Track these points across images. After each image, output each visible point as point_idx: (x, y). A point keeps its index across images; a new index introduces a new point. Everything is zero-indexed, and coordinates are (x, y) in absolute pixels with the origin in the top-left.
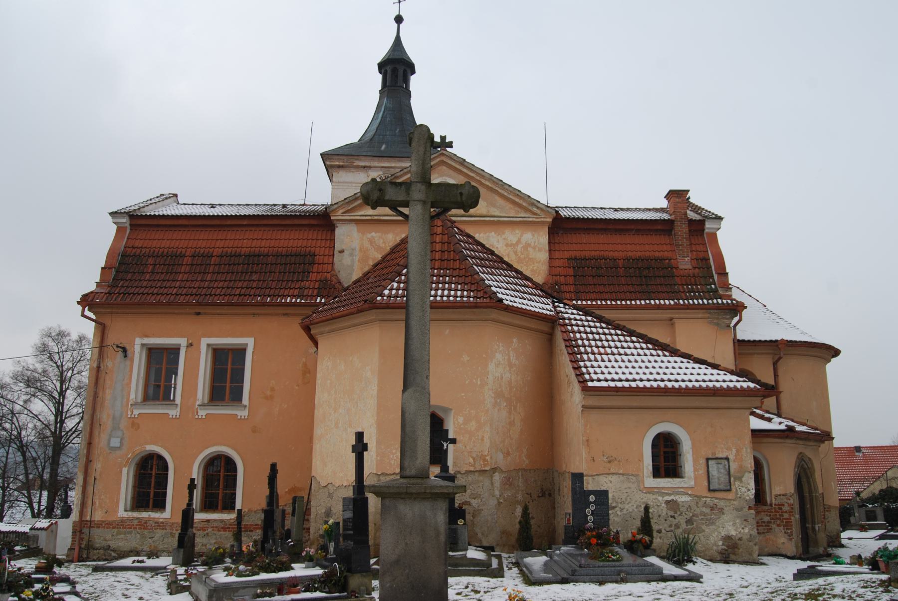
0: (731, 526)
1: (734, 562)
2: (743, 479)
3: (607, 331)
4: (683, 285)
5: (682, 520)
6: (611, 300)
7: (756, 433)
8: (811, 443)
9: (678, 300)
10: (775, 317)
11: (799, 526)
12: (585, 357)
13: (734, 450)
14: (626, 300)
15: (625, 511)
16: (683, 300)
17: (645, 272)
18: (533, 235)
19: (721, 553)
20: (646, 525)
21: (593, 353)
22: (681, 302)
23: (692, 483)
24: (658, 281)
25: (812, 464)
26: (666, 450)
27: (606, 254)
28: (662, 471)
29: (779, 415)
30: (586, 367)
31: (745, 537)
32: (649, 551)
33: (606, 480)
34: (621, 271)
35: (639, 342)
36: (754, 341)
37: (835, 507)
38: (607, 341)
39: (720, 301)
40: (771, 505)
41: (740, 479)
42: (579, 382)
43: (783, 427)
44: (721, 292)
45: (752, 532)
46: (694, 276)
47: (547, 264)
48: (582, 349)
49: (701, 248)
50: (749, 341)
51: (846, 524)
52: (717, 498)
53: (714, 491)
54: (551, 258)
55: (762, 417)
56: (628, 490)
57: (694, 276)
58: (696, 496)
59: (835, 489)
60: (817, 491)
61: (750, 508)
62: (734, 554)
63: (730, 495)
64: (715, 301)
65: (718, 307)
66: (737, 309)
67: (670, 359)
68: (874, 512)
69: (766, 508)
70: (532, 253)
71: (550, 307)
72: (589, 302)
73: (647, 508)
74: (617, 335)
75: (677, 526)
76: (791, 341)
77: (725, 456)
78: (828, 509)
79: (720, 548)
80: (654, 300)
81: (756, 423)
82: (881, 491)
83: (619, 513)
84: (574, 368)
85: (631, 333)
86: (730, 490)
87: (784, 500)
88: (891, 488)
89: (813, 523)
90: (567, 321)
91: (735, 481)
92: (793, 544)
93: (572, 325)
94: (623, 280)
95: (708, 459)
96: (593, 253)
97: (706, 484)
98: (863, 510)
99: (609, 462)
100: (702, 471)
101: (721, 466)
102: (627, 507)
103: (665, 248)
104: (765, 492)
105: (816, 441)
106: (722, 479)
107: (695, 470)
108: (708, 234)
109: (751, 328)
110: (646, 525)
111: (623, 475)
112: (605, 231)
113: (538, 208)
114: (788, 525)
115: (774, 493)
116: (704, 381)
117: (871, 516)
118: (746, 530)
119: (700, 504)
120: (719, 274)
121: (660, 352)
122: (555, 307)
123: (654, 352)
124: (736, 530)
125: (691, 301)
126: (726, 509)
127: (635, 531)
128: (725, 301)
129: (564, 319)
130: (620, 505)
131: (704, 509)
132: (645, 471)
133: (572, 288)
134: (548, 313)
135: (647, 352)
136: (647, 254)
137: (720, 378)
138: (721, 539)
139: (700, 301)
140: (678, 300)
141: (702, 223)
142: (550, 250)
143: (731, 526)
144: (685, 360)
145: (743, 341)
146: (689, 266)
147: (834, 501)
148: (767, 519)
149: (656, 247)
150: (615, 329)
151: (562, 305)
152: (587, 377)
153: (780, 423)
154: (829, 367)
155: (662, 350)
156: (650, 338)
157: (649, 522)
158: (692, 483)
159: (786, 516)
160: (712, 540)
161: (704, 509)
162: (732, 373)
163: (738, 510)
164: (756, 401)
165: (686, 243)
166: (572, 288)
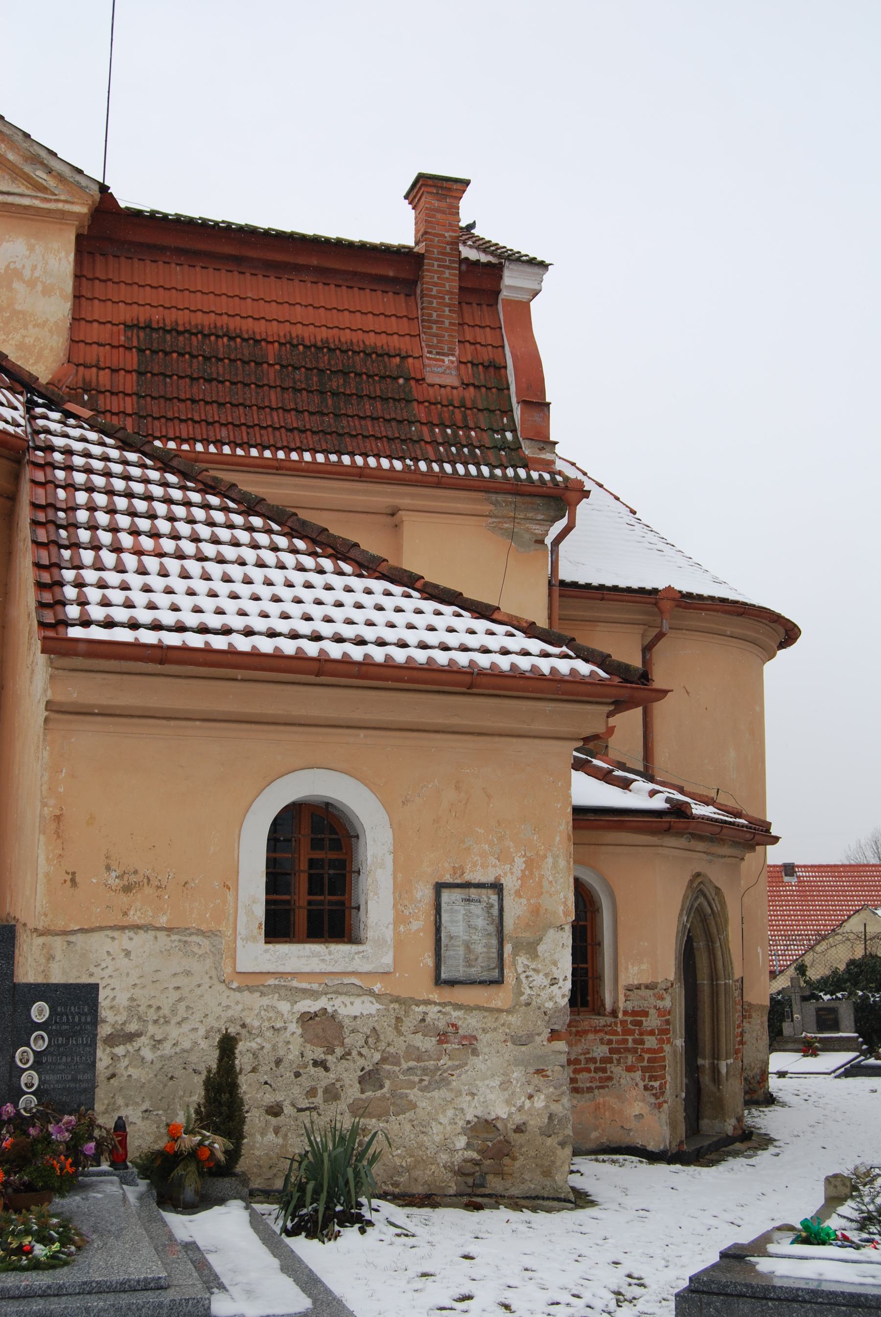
0: (499, 1085)
1: (496, 1200)
2: (541, 949)
3: (177, 494)
4: (431, 425)
5: (347, 1075)
6: (234, 445)
7: (585, 817)
8: (725, 850)
9: (416, 460)
10: (655, 540)
11: (681, 1067)
12: (87, 556)
13: (520, 863)
14: (275, 448)
15: (167, 1049)
16: (429, 461)
17: (336, 383)
18: (31, 249)
19: (460, 1172)
20: (222, 1102)
21: (117, 549)
22: (423, 466)
23: (387, 960)
24: (368, 408)
25: (723, 904)
26: (318, 855)
27: (234, 324)
28: (301, 920)
29: (651, 779)
30: (80, 584)
31: (535, 1123)
32: (225, 1184)
33: (109, 946)
34: (271, 375)
35: (269, 531)
36: (602, 587)
37: (761, 1007)
38: (172, 519)
39: (522, 473)
40: (614, 1013)
41: (531, 948)
42: (42, 625)
43: (658, 803)
44: (528, 450)
45: (556, 1108)
46: (463, 405)
47: (66, 335)
48: (84, 535)
49: (486, 336)
50: (588, 586)
51: (777, 1040)
52: (458, 1007)
53: (452, 983)
54: (76, 319)
55: (606, 777)
56: (180, 981)
57: (463, 405)
58: (397, 1000)
59: (760, 967)
60: (728, 975)
61: (554, 1035)
62: (501, 1174)
63: (499, 998)
64: (510, 472)
65: (518, 490)
66: (562, 497)
67: (358, 584)
68: (833, 1011)
69: (602, 1021)
70: (24, 298)
71: (19, 415)
72: (172, 445)
73: (227, 1046)
74: (207, 506)
75: (332, 1094)
76: (689, 595)
77: (489, 878)
78: (747, 1011)
79: (458, 1158)
80: (352, 454)
81: (589, 791)
82: (852, 962)
83: (148, 1054)
84: (41, 586)
85: (251, 506)
86: (499, 981)
87: (648, 1000)
88: (873, 957)
89: (716, 1056)
90: (58, 457)
91: (515, 954)
92: (664, 1117)
93: (69, 468)
94: (274, 398)
95: (439, 887)
96: (199, 318)
97: (430, 962)
98: (812, 1005)
99: (127, 889)
100: (421, 924)
101: (477, 909)
102: (174, 1032)
103: (393, 325)
104: (599, 978)
105: (735, 844)
106: (479, 949)
107: (400, 919)
108: (508, 302)
109: (592, 554)
110: (222, 1102)
111: (169, 930)
112: (237, 263)
113: (50, 171)
114: (653, 1069)
115: (623, 981)
116: (445, 648)
117: (827, 1020)
118: (540, 1102)
119: (408, 1024)
120: (525, 403)
121: (327, 564)
122: (32, 418)
123: (308, 562)
124: (508, 1102)
125: (448, 468)
126: (484, 1038)
127: (180, 1119)
128: (535, 475)
129: (51, 449)
130: (152, 1029)
131: (418, 1041)
132: (242, 919)
133: (129, 405)
134: (11, 429)
135: (289, 559)
136: (346, 336)
137: (493, 643)
138: (464, 1132)
139: (473, 469)
140: (416, 460)
141: (494, 271)
142: (77, 297)
143: (499, 1085)
144: (397, 590)
145: (574, 585)
146: (452, 380)
147: (762, 991)
148: (601, 1051)
149: (370, 322)
150: (202, 492)
151: (56, 416)
152: (73, 612)
153: (653, 793)
154: (770, 669)
155: (335, 556)
156: (304, 523)
157: (233, 1086)
158: (387, 960)
159: (651, 1042)
160: (437, 1133)
161: (418, 1041)
162: (530, 630)
163: (518, 1041)
164: (590, 718)
165: (449, 317)
166: (129, 405)
